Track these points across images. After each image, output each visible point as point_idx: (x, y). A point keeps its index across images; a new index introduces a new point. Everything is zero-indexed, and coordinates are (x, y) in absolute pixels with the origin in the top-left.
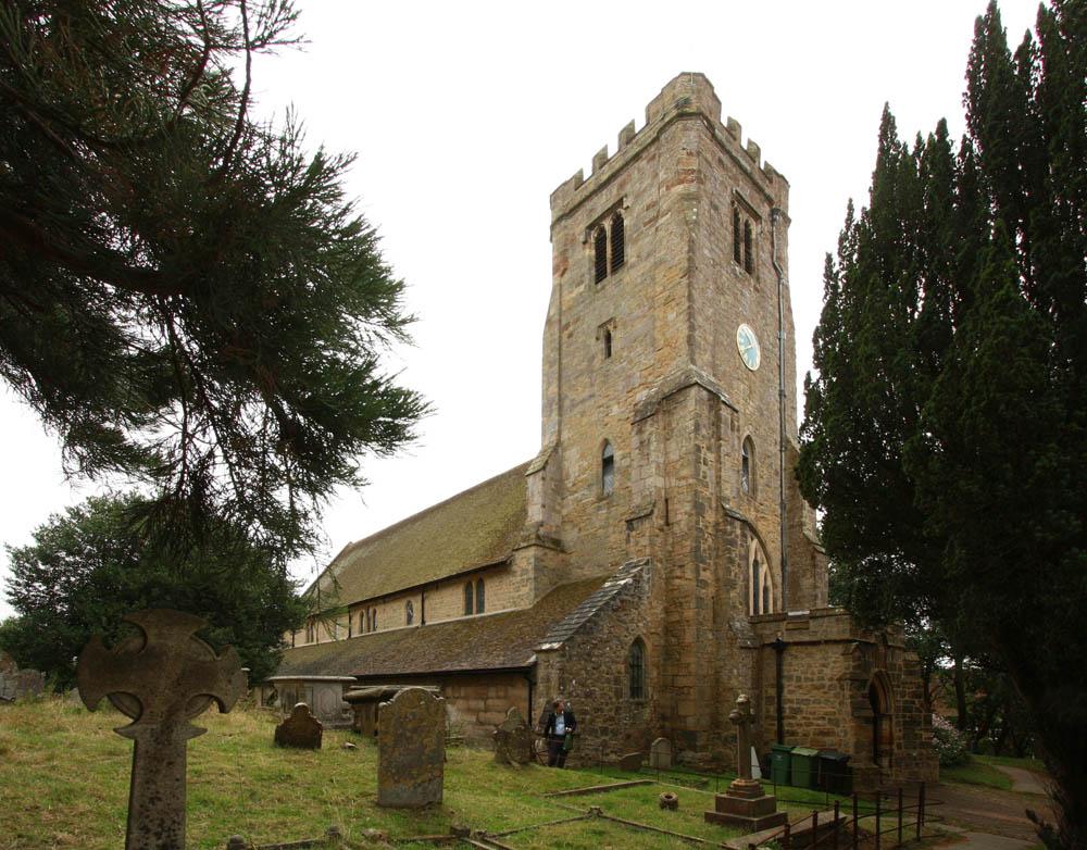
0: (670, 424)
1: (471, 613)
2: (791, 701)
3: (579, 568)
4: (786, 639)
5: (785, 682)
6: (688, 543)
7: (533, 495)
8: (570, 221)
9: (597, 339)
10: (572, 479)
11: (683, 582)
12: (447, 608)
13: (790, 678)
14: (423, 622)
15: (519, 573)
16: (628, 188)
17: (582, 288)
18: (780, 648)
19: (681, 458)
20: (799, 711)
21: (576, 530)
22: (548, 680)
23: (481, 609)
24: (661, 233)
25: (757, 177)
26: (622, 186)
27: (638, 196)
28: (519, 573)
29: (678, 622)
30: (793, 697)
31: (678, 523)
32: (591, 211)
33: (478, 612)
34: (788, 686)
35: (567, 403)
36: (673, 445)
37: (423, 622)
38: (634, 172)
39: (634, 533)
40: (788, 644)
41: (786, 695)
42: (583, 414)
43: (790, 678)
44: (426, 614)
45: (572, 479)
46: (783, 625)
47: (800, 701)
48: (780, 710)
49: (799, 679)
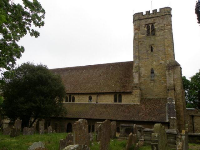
0: (174, 71)
1: (117, 102)
2: (196, 127)
3: (146, 94)
4: (194, 115)
5: (194, 123)
6: (180, 95)
7: (135, 77)
8: (140, 21)
9: (149, 47)
10: (143, 74)
11: (179, 103)
12: (109, 100)
13: (195, 122)
14: (97, 102)
15: (134, 95)
16: (156, 21)
17: (144, 35)
18: (193, 116)
19: (177, 78)
20: (197, 129)
21: (144, 86)
22: (173, 125)
23: (120, 101)
24: (165, 33)
25: (153, 16)
26: (154, 20)
27: (159, 24)
28: (134, 95)
29: (179, 111)
30: (196, 126)
31: (177, 91)
32: (146, 21)
33: (119, 102)
34: (195, 124)
35: (141, 58)
36: (175, 75)
37: (97, 102)
38: (157, 18)
39: (169, 92)
40: (195, 116)
41: (195, 126)
42: (145, 61)
43: (195, 122)
44: (98, 100)
45: (143, 74)
46: (193, 112)
47: (197, 127)
48: (194, 129)
49: (197, 123)
